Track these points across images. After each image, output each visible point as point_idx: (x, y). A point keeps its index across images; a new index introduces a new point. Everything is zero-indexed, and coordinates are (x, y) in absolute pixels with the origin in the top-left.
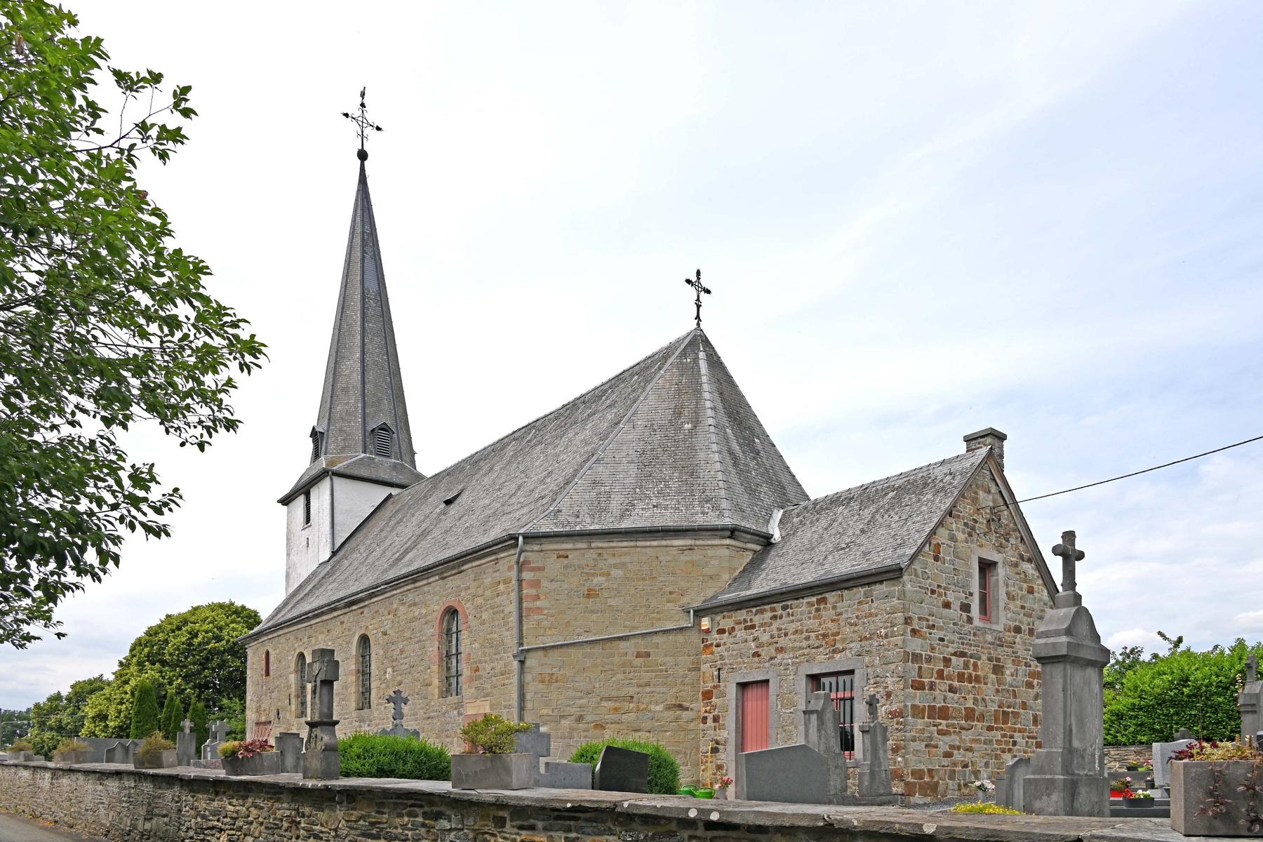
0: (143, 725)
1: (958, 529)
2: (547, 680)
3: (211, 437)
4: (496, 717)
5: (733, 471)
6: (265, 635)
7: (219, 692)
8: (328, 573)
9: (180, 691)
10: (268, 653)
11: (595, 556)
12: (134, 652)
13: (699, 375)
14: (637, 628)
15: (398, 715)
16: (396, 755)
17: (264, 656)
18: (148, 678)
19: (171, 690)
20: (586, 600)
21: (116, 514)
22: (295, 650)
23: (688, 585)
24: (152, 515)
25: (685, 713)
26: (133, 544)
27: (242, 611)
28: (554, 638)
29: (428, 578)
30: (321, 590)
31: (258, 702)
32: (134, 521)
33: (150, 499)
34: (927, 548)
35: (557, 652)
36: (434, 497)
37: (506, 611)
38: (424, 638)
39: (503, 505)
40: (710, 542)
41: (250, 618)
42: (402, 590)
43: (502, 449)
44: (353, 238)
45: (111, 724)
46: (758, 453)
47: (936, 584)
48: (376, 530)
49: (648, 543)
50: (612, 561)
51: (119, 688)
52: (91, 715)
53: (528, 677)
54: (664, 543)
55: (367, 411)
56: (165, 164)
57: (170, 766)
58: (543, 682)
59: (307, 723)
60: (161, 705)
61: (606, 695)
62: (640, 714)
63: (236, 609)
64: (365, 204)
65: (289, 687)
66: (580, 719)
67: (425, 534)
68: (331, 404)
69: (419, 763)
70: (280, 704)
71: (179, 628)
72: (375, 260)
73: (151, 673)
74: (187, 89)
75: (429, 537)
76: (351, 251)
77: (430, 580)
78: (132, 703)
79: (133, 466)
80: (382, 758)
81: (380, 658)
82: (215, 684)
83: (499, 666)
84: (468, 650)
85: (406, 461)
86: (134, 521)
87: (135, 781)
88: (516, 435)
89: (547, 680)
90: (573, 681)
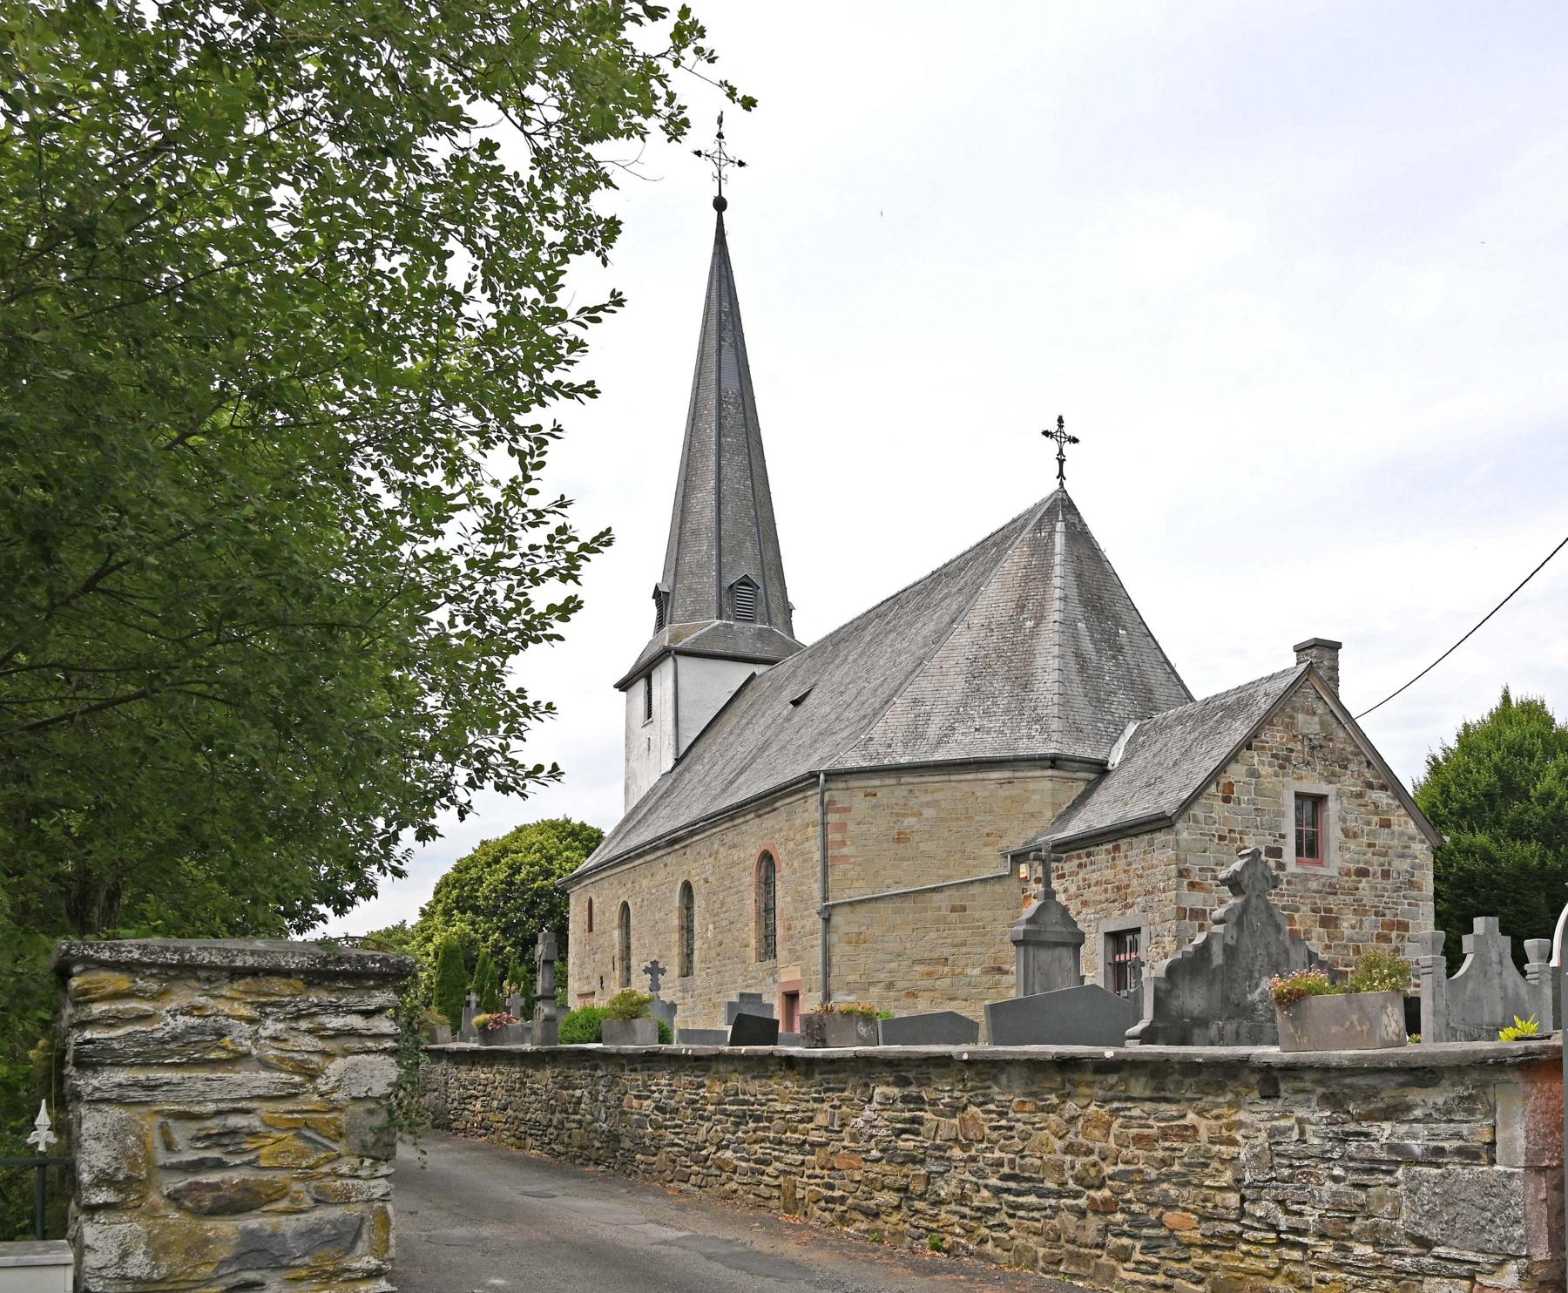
1: (1262, 763)
5: (1077, 679)
6: (589, 877)
11: (905, 793)
13: (1053, 554)
14: (951, 877)
15: (655, 986)
19: (484, 949)
23: (1007, 825)
25: (1005, 977)
26: (384, 882)
27: (581, 831)
34: (1213, 788)
35: (866, 907)
40: (1030, 774)
41: (587, 839)
46: (1120, 650)
47: (1227, 829)
49: (962, 777)
50: (924, 798)
53: (834, 938)
54: (980, 776)
55: (724, 560)
58: (850, 943)
60: (471, 969)
61: (919, 957)
63: (573, 829)
68: (678, 552)
71: (497, 861)
72: (736, 349)
73: (461, 926)
78: (435, 968)
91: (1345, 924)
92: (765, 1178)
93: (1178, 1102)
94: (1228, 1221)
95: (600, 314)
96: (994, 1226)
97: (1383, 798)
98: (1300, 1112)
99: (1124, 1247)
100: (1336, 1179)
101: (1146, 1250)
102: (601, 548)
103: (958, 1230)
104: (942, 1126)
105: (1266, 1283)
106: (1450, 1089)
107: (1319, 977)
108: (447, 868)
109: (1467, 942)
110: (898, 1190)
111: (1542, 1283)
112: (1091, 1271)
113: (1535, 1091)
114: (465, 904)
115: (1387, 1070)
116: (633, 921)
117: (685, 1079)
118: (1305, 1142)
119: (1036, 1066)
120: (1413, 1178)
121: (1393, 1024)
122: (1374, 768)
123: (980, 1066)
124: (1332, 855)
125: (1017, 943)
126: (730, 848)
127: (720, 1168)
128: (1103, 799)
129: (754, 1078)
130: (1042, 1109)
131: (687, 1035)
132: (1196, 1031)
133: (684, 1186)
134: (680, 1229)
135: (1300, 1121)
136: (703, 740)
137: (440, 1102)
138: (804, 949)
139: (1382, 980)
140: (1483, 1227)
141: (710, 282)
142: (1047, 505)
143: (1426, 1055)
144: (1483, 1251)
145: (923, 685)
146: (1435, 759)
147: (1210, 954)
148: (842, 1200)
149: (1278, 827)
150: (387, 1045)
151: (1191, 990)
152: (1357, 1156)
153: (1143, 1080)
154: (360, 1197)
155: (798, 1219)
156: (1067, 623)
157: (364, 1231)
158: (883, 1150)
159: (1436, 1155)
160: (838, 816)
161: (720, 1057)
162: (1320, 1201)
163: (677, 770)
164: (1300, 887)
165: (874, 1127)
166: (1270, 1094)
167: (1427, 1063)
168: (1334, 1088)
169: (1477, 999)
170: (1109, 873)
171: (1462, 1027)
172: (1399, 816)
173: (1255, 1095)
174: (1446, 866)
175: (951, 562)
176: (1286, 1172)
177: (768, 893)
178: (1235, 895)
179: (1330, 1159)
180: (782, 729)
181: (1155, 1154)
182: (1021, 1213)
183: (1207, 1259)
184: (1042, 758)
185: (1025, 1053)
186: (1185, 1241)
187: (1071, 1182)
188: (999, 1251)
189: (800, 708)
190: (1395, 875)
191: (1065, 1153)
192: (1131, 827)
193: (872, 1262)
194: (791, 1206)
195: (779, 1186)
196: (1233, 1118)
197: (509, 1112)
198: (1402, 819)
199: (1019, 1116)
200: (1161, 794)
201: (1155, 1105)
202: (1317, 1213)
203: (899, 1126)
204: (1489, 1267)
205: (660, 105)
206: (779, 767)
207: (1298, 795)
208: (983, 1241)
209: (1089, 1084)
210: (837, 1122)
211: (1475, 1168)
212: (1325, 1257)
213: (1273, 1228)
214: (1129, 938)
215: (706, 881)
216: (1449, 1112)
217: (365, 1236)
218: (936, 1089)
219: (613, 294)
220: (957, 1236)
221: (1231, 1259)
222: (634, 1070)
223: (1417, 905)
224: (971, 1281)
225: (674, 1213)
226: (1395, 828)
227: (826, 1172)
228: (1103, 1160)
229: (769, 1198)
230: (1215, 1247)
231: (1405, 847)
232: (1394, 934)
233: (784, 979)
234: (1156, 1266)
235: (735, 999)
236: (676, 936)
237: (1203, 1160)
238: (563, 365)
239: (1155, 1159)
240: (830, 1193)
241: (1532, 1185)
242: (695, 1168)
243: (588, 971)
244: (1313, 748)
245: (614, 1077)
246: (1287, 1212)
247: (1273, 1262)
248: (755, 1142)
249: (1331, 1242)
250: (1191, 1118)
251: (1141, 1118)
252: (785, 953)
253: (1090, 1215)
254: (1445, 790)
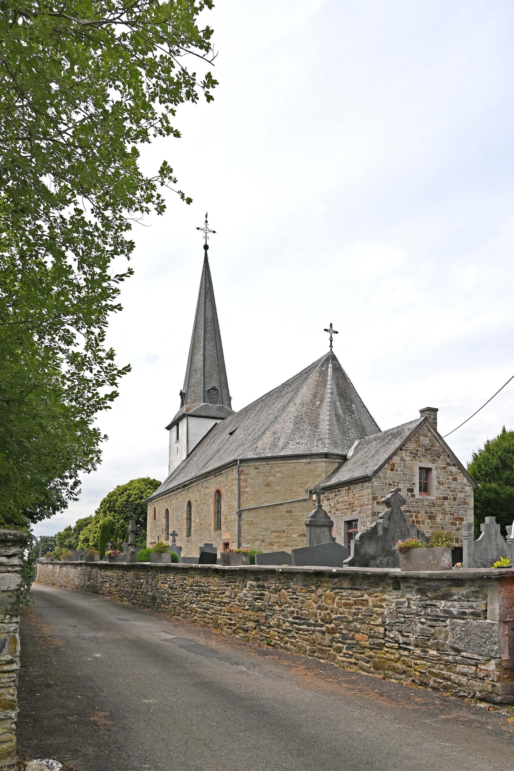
1: (406, 455)
5: (336, 424)
11: (270, 468)
13: (327, 376)
15: (174, 541)
19: (118, 526)
23: (308, 480)
34: (387, 466)
40: (317, 460)
41: (154, 484)
45: (91, 544)
46: (353, 412)
47: (392, 481)
49: (291, 461)
50: (277, 470)
52: (82, 539)
53: (242, 522)
54: (298, 461)
55: (206, 381)
61: (274, 530)
62: (288, 538)
66: (263, 541)
71: (123, 493)
91: (438, 518)
92: (207, 615)
93: (361, 590)
94: (379, 638)
95: (124, 278)
96: (290, 637)
97: (454, 469)
98: (408, 596)
99: (339, 647)
100: (422, 623)
101: (348, 648)
102: (126, 372)
103: (277, 638)
104: (272, 597)
105: (394, 664)
106: (469, 588)
107: (419, 542)
108: (105, 496)
109: (482, 526)
110: (255, 621)
111: (505, 669)
112: (327, 656)
113: (503, 590)
114: (111, 509)
115: (443, 579)
116: (170, 516)
117: (179, 577)
118: (410, 608)
119: (307, 574)
120: (453, 624)
121: (447, 561)
122: (450, 458)
123: (286, 574)
124: (433, 491)
125: (307, 525)
127: (191, 611)
128: (344, 469)
129: (204, 577)
130: (309, 592)
131: (185, 560)
132: (371, 561)
133: (178, 617)
134: (173, 635)
135: (408, 599)
136: (197, 448)
137: (95, 583)
138: (231, 527)
139: (443, 543)
140: (481, 645)
141: (202, 277)
142: (326, 357)
143: (459, 574)
144: (481, 655)
145: (277, 427)
146: (475, 454)
147: (377, 531)
148: (235, 625)
149: (412, 480)
150: (17, 569)
151: (369, 545)
152: (431, 614)
153: (347, 581)
154: (4, 631)
155: (218, 631)
156: (332, 403)
157: (6, 645)
158: (250, 606)
159: (462, 615)
160: (244, 476)
161: (191, 568)
162: (416, 632)
163: (187, 459)
164: (420, 504)
165: (247, 597)
166: (397, 588)
167: (460, 577)
168: (422, 586)
169: (486, 549)
170: (346, 498)
171: (479, 561)
172: (460, 476)
173: (391, 588)
174: (480, 496)
175: (290, 380)
176: (403, 619)
177: (219, 505)
178: (388, 507)
179: (420, 615)
180: (225, 444)
181: (352, 610)
182: (301, 632)
183: (371, 653)
184: (322, 454)
185: (303, 569)
186: (363, 646)
187: (319, 620)
188: (292, 647)
189: (232, 436)
190: (458, 499)
191: (318, 609)
192: (355, 480)
193: (243, 650)
194: (216, 626)
195: (212, 619)
196: (382, 597)
197: (118, 587)
198: (462, 477)
199: (300, 594)
200: (367, 467)
201: (352, 591)
202: (415, 636)
203: (256, 596)
204: (483, 661)
205: (154, 199)
206: (224, 458)
207: (421, 468)
208: (286, 643)
209: (327, 582)
210: (233, 595)
211: (479, 621)
212: (417, 655)
213: (397, 642)
214: (354, 523)
215: (196, 501)
216: (468, 597)
217: (6, 647)
218: (270, 583)
219: (129, 270)
220: (277, 640)
221: (380, 654)
222: (161, 573)
223: (467, 511)
224: (279, 659)
225: (172, 628)
226: (459, 481)
227: (229, 614)
228: (332, 612)
229: (209, 623)
230: (374, 649)
231: (462, 488)
232: (458, 522)
233: (224, 538)
234: (352, 655)
235: (203, 546)
236: (185, 521)
237: (370, 614)
238: (110, 299)
239: (352, 612)
240: (230, 622)
241: (502, 629)
242: (182, 611)
243: (154, 534)
244: (426, 450)
245: (155, 575)
246: (403, 636)
247: (397, 656)
248: (204, 601)
249: (420, 649)
250: (366, 597)
251: (346, 596)
252: (224, 528)
253: (326, 634)
254: (479, 466)
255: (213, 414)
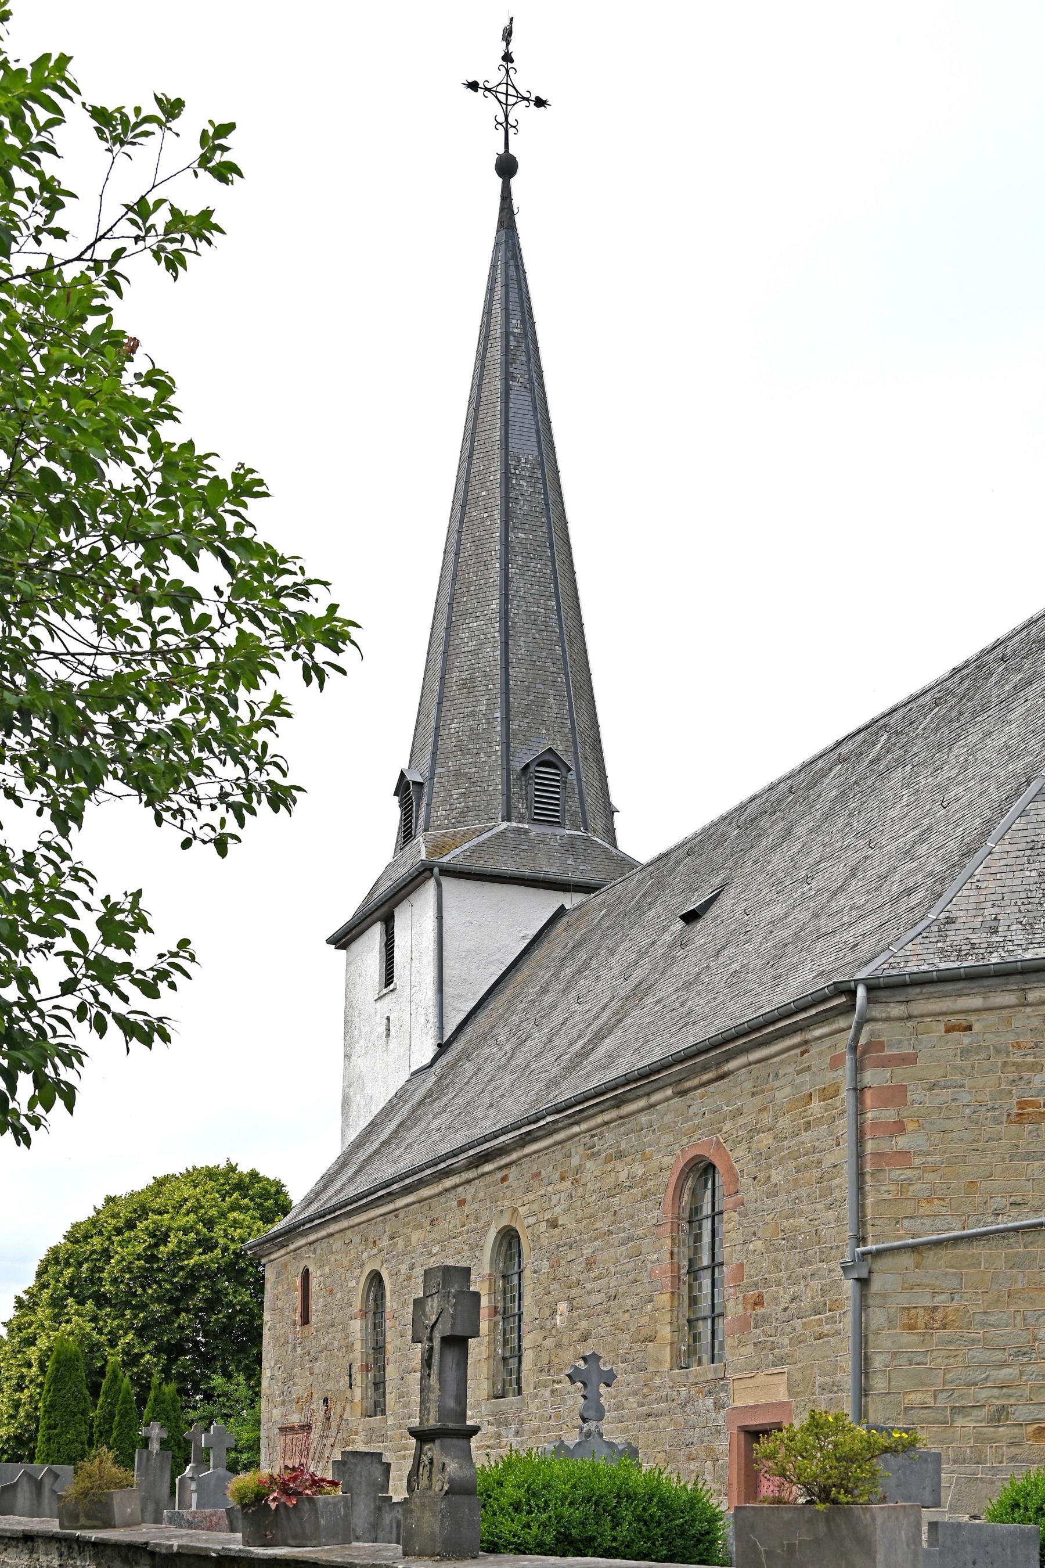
0: (60, 1435)
2: (921, 1322)
3: (242, 824)
4: (836, 1419)
7: (206, 1360)
8: (429, 1094)
9: (132, 1359)
10: (306, 1275)
12: (45, 1277)
15: (593, 1411)
16: (597, 1504)
17: (298, 1281)
18: (72, 1333)
19: (115, 1358)
20: (1014, 1128)
21: (71, 1002)
22: (362, 1265)
24: (138, 999)
28: (938, 1224)
29: (648, 1094)
30: (417, 1131)
31: (284, 1382)
32: (104, 1013)
33: (136, 967)
35: (947, 1254)
36: (658, 908)
37: (827, 1164)
38: (640, 1232)
39: (816, 916)
42: (592, 1123)
43: (813, 784)
44: (485, 350)
48: (532, 991)
51: (15, 1353)
53: (877, 1318)
55: (514, 726)
56: (175, 278)
57: (127, 1525)
58: (912, 1327)
59: (413, 1432)
60: (95, 1390)
63: (241, 1180)
64: (512, 272)
65: (350, 1348)
66: (1000, 1415)
67: (640, 992)
69: (645, 1523)
70: (329, 1386)
71: (131, 1225)
72: (532, 392)
74: (226, 129)
75: (650, 1000)
76: (481, 380)
77: (655, 1098)
78: (41, 1385)
79: (106, 901)
80: (566, 1511)
81: (543, 1278)
82: (196, 1343)
83: (810, 1292)
84: (737, 1257)
85: (594, 831)
86: (104, 1013)
87: (61, 1555)
88: (844, 750)
89: (921, 1322)
90: (983, 1324)
126: (608, 1160)
189: (699, 925)
233: (741, 1401)
255: (551, 870)
